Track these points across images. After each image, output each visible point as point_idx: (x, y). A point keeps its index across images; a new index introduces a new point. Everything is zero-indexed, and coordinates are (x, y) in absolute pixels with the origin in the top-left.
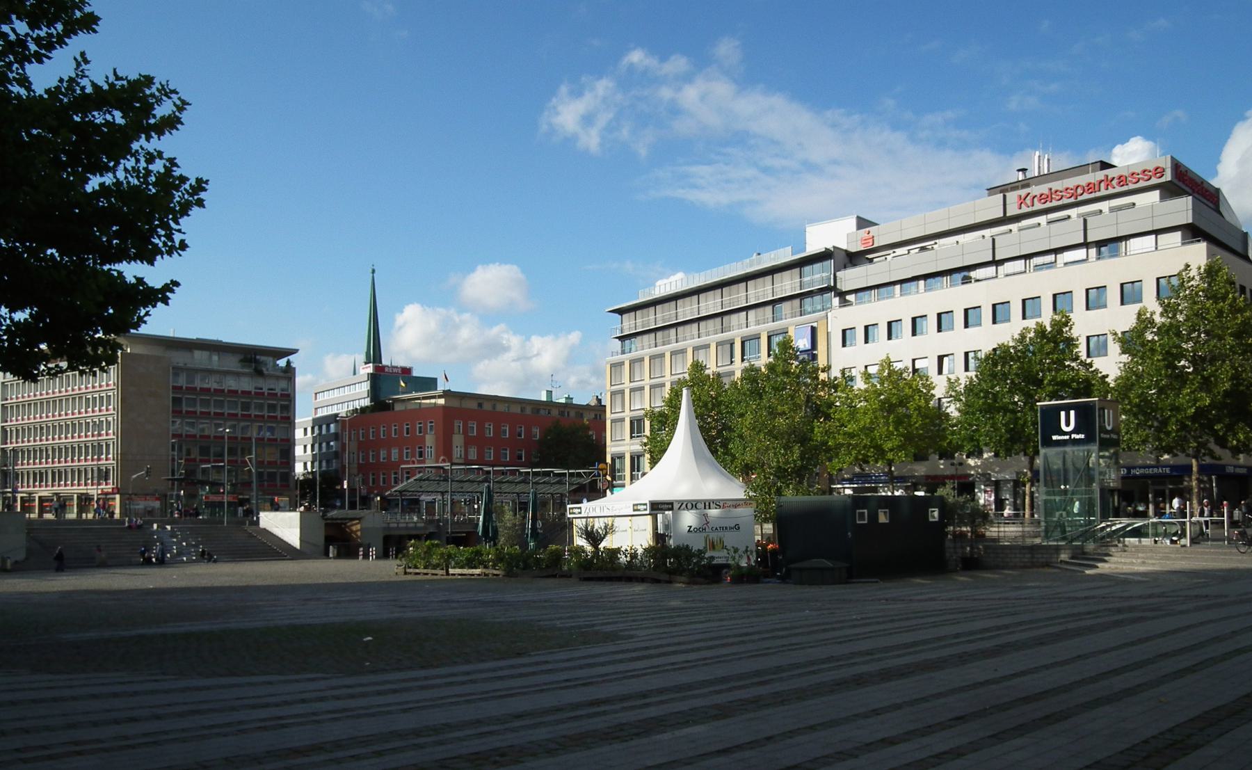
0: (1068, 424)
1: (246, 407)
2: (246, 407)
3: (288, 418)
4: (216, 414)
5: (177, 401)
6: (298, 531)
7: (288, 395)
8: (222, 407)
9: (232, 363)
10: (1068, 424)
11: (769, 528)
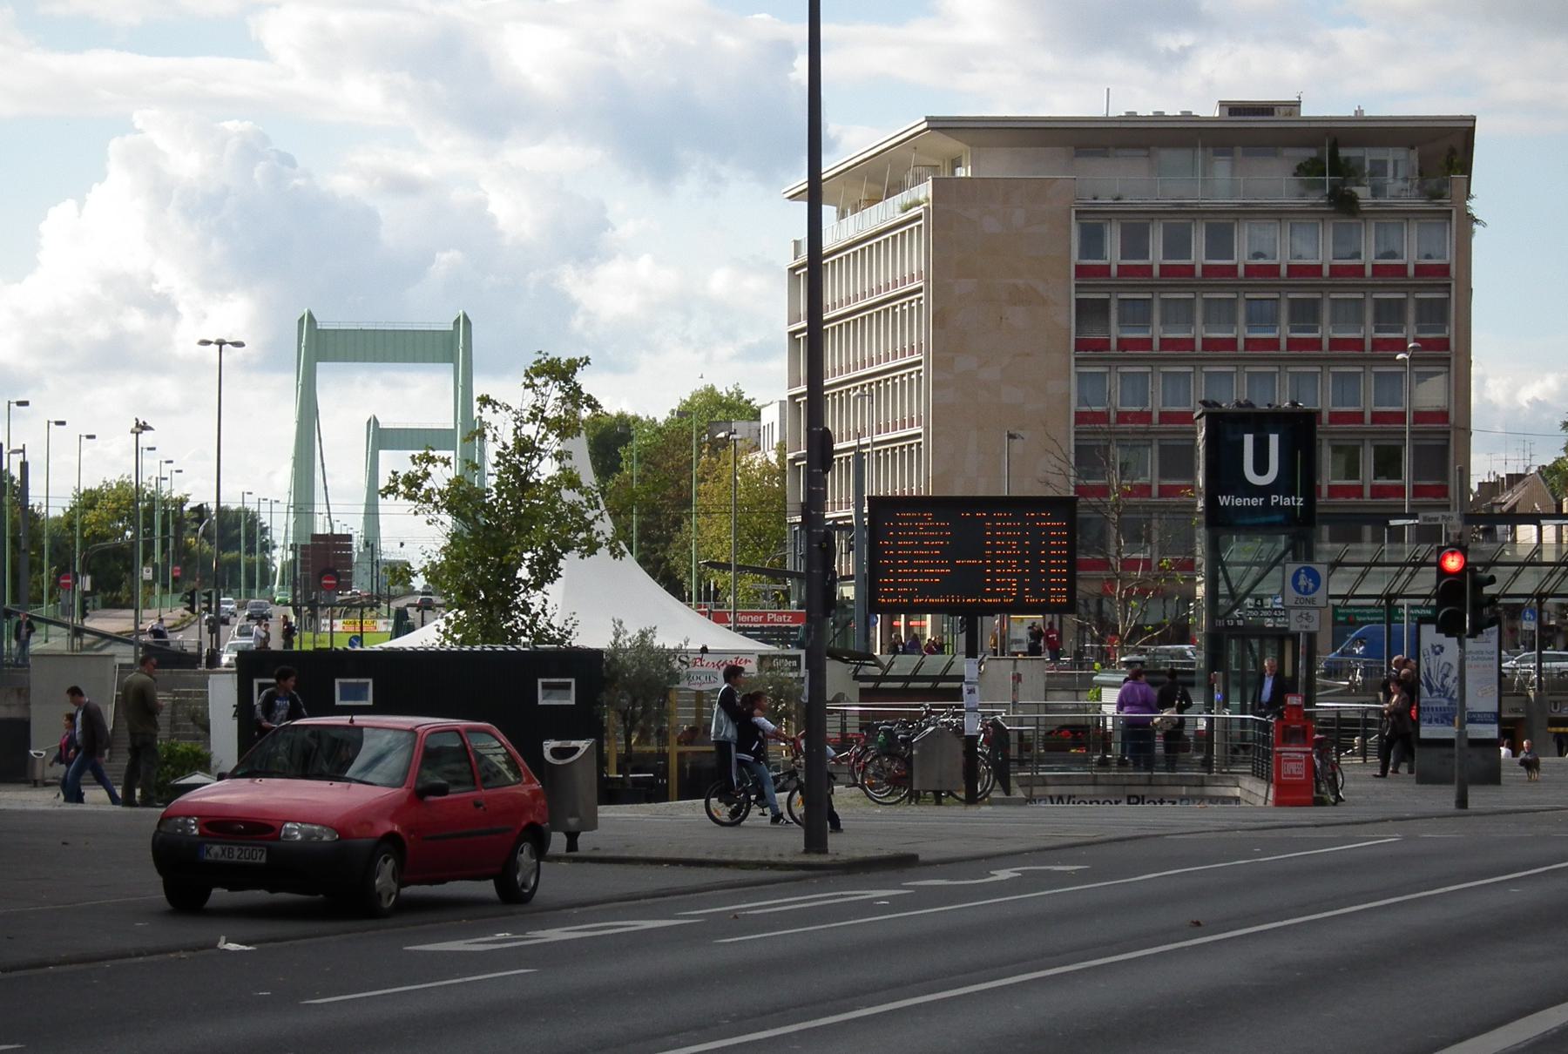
0: (1261, 468)
1: (1305, 313)
2: (1305, 313)
3: (1444, 344)
4: (1208, 344)
5: (1090, 311)
6: (294, 427)
7: (1444, 270)
8: (1146, 322)
9: (1274, 180)
10: (1261, 468)
11: (448, 519)
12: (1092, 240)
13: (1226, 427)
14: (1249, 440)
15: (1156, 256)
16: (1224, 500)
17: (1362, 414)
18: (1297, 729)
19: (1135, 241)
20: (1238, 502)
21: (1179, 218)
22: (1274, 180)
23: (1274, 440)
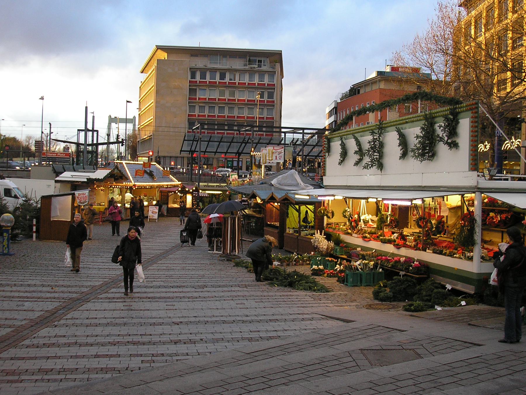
12: (193, 76)
15: (208, 79)
17: (215, 116)
18: (309, 162)
19: (203, 76)
21: (213, 71)
22: (238, 64)
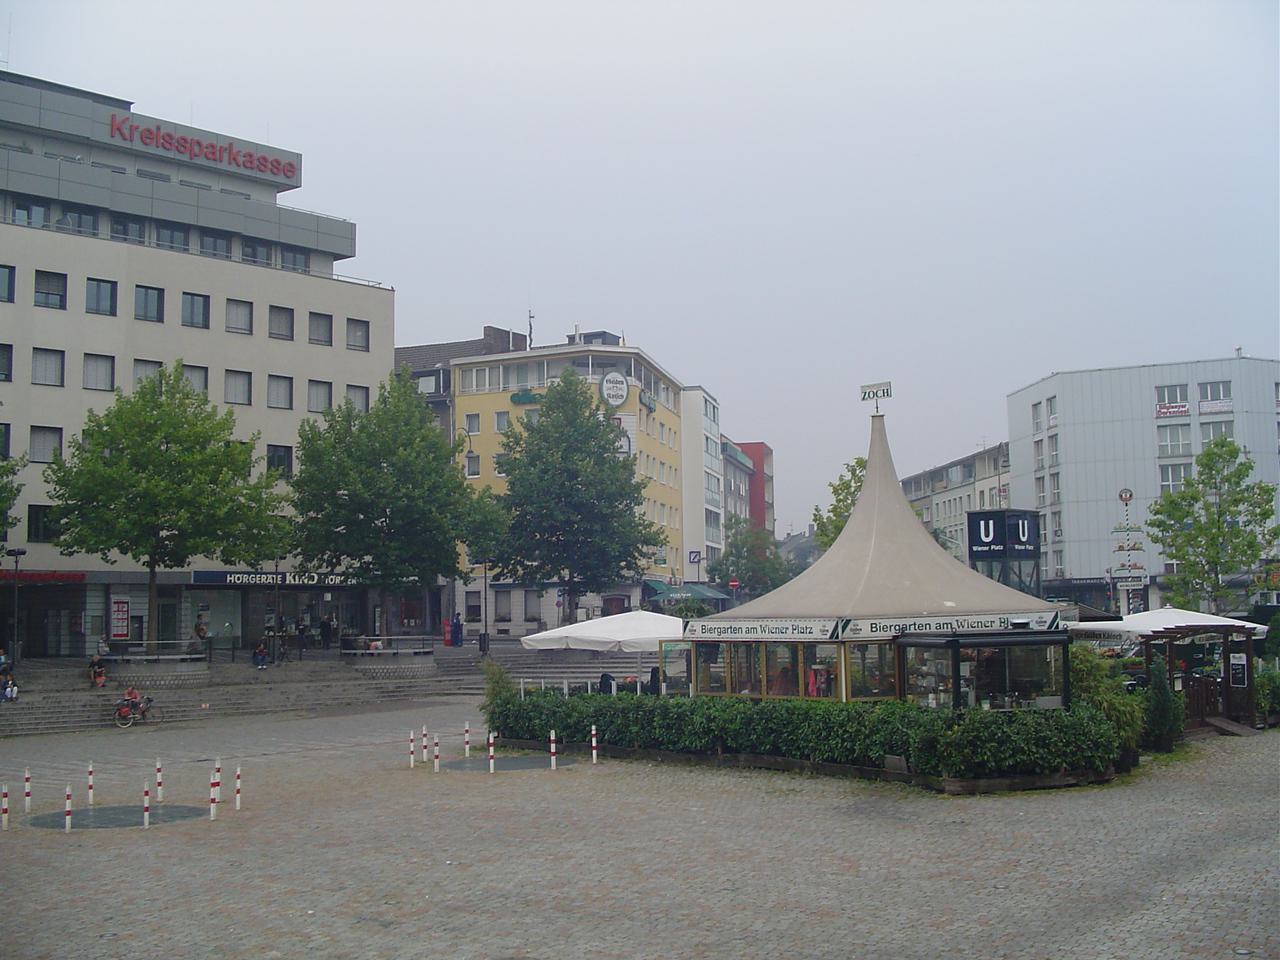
0: (987, 536)
10: (987, 536)
13: (974, 519)
14: (982, 523)
16: (975, 548)
20: (980, 549)
23: (991, 522)
